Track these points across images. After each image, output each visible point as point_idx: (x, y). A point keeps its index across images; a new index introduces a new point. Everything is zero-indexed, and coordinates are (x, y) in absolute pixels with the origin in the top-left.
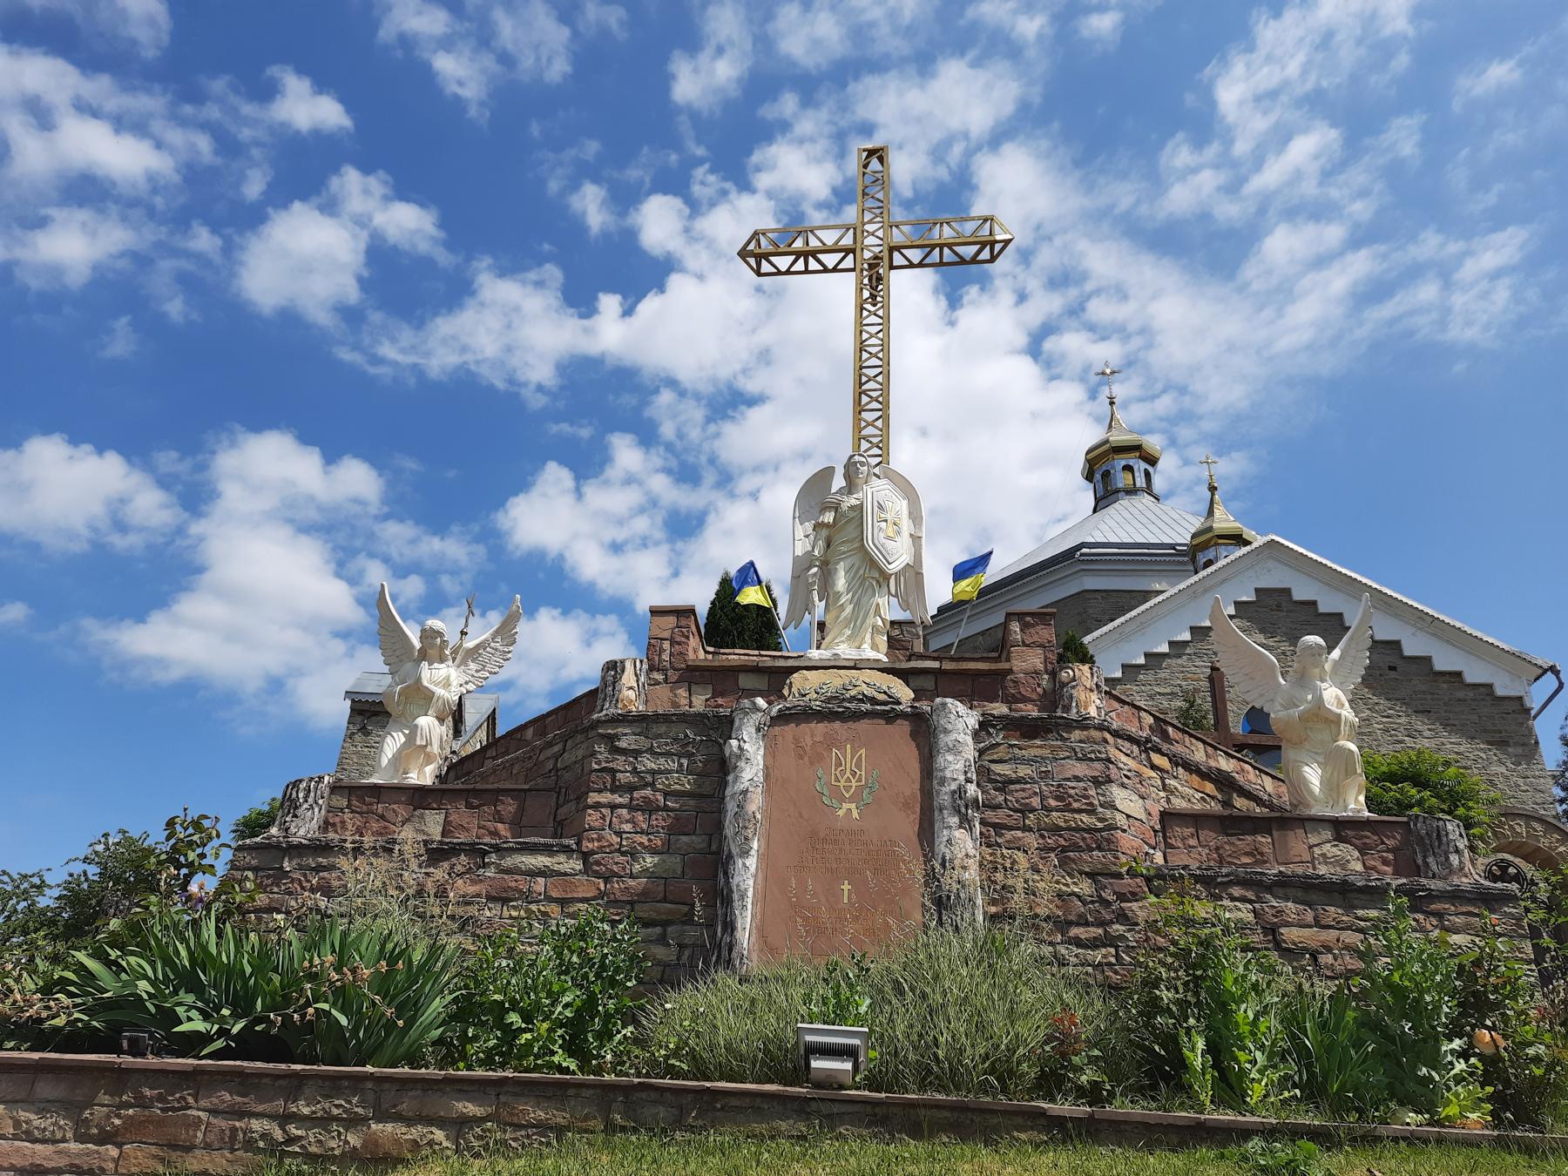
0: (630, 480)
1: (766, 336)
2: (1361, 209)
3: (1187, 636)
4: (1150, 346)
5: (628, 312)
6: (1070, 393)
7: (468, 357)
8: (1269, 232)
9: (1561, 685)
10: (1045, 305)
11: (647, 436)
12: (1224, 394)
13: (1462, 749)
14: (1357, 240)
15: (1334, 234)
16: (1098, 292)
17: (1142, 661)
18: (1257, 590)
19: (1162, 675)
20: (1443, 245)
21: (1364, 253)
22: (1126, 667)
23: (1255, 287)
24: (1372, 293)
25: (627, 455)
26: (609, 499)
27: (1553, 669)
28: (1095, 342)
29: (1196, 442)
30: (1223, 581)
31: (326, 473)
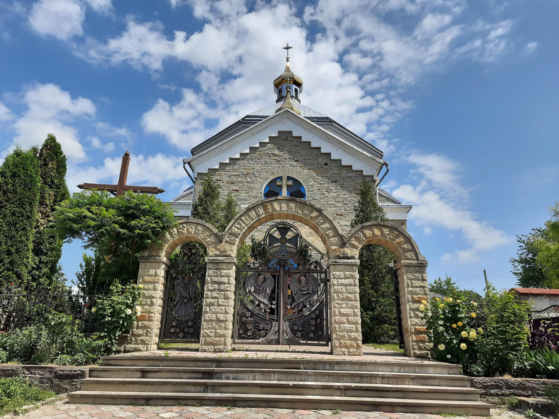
0: (191, 106)
1: (240, 51)
2: (457, 10)
3: (247, 151)
4: (382, 59)
5: (187, 38)
6: (353, 77)
7: (128, 57)
8: (425, 17)
9: (388, 170)
10: (344, 42)
11: (197, 88)
12: (406, 79)
13: (346, 196)
14: (454, 23)
15: (447, 19)
16: (365, 38)
17: (228, 161)
18: (279, 132)
19: (236, 167)
20: (484, 26)
21: (457, 28)
22: (221, 164)
23: (419, 38)
24: (458, 42)
25: (189, 96)
26: (182, 113)
27: (385, 163)
28: (361, 58)
29: (396, 97)
30: (266, 128)
31: (73, 103)
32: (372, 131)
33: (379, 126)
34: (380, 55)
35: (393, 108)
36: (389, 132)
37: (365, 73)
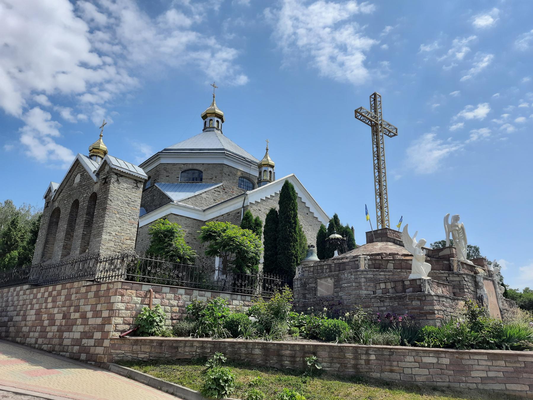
15: (188, 22)
24: (192, 47)
32: (92, 93)
33: (101, 90)
34: (118, 19)
35: (118, 77)
36: (109, 102)
37: (99, 29)
